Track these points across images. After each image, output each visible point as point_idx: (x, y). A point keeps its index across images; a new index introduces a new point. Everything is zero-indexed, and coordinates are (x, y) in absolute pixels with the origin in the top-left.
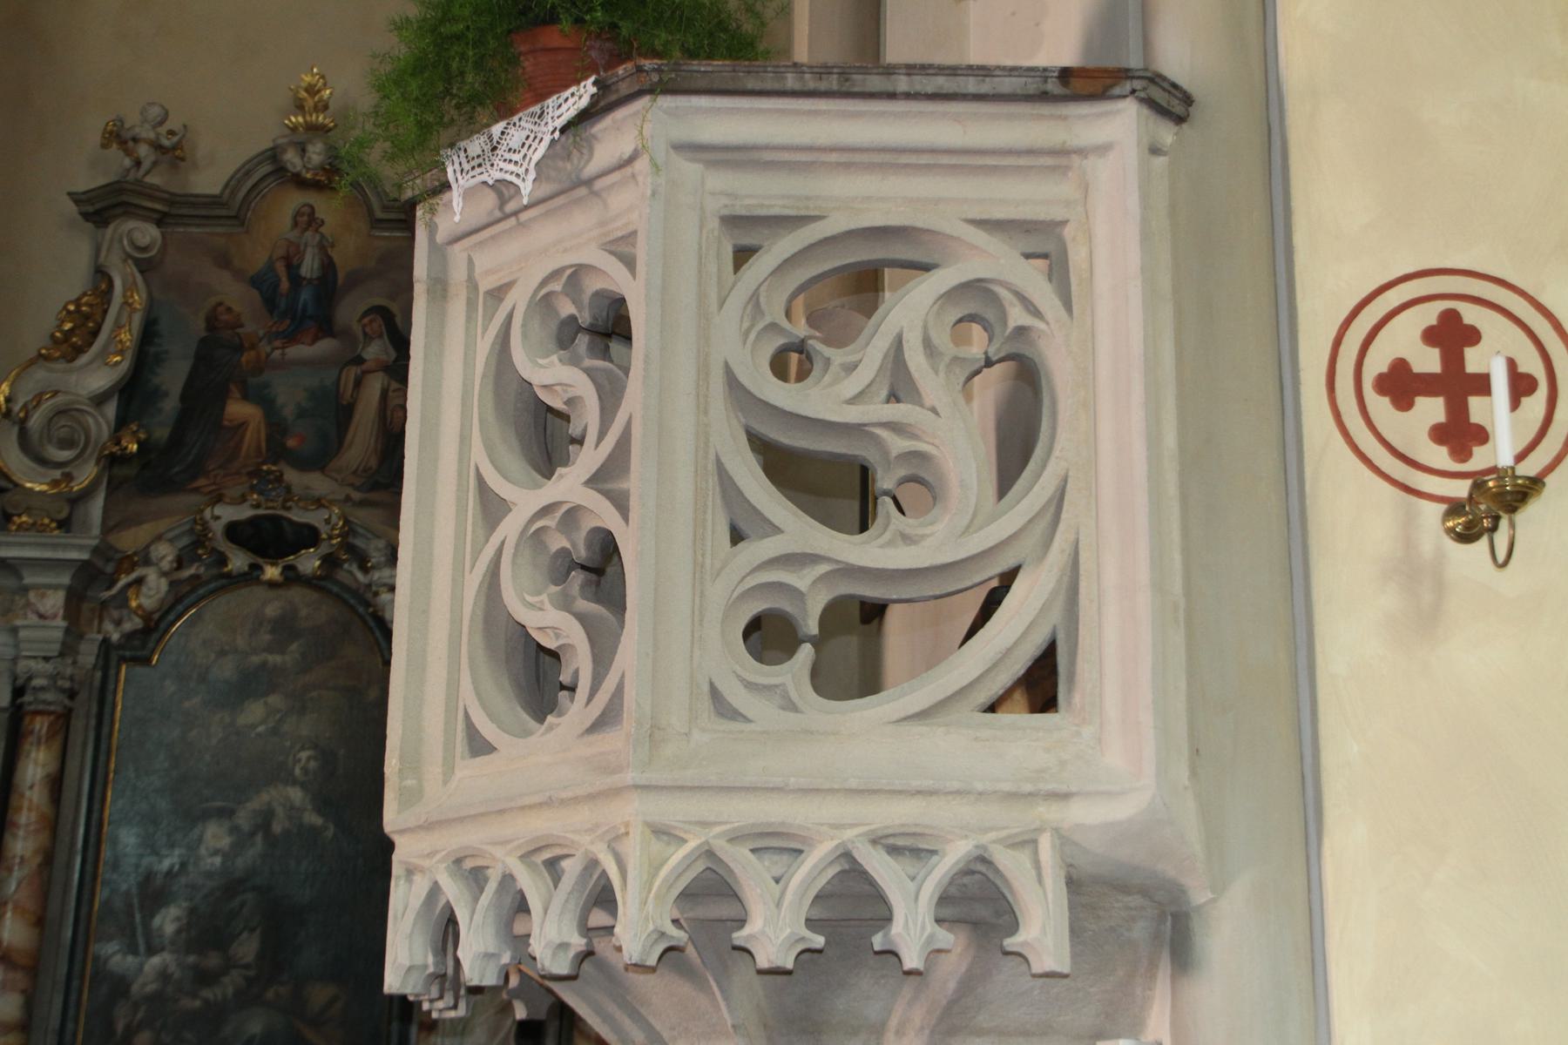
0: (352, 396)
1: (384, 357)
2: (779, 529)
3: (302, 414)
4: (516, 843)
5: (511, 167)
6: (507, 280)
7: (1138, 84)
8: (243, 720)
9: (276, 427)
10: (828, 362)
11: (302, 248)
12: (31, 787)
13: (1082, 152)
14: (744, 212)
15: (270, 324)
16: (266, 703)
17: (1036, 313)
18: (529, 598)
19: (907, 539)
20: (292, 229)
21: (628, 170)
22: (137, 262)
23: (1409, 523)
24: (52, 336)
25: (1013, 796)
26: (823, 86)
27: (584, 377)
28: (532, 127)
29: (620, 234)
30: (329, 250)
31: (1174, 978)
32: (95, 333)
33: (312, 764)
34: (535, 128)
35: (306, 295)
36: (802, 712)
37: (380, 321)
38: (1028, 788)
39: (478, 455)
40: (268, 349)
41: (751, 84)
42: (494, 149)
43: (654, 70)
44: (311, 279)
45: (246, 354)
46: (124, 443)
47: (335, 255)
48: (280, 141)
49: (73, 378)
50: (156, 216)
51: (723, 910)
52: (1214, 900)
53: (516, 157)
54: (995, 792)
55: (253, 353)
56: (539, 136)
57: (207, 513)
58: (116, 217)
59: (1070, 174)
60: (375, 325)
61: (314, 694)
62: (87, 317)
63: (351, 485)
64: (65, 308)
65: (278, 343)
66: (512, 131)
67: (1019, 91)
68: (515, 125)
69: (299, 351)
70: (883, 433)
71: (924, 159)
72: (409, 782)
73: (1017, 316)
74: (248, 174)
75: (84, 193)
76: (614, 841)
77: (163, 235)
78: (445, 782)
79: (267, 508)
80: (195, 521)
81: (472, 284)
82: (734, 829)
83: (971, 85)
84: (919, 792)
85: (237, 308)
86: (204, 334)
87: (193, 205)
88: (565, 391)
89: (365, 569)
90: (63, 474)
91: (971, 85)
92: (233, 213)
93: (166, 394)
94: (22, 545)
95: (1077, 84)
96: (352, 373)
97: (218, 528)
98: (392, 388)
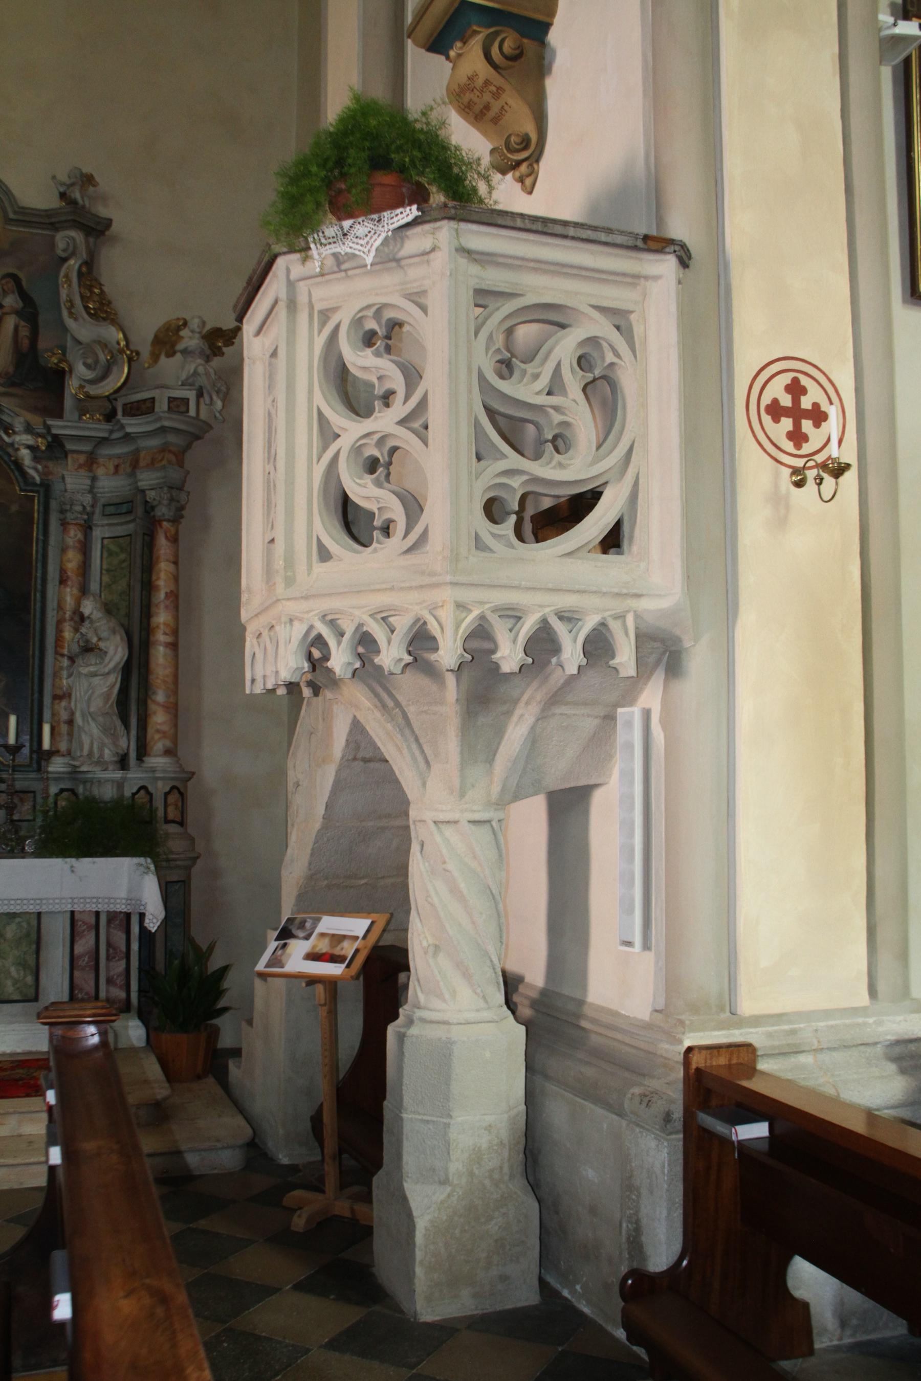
2: (505, 456)
4: (369, 608)
5: (359, 247)
6: (335, 305)
7: (677, 248)
10: (524, 372)
13: (646, 278)
14: (486, 288)
17: (617, 355)
18: (358, 481)
19: (561, 465)
21: (426, 257)
23: (777, 475)
25: (618, 595)
26: (534, 227)
27: (394, 366)
28: (373, 227)
29: (415, 290)
31: (666, 680)
34: (375, 228)
36: (516, 549)
38: (625, 591)
39: (319, 400)
41: (500, 222)
42: (345, 235)
43: (453, 207)
51: (486, 645)
52: (694, 646)
53: (361, 242)
54: (611, 593)
56: (378, 232)
59: (638, 288)
66: (357, 226)
67: (625, 244)
68: (359, 223)
70: (551, 411)
71: (575, 271)
72: (289, 574)
73: (610, 358)
76: (432, 610)
78: (309, 574)
81: (311, 306)
82: (496, 606)
83: (603, 237)
84: (578, 591)
88: (378, 372)
89: (9, 435)
91: (603, 237)
95: (651, 244)
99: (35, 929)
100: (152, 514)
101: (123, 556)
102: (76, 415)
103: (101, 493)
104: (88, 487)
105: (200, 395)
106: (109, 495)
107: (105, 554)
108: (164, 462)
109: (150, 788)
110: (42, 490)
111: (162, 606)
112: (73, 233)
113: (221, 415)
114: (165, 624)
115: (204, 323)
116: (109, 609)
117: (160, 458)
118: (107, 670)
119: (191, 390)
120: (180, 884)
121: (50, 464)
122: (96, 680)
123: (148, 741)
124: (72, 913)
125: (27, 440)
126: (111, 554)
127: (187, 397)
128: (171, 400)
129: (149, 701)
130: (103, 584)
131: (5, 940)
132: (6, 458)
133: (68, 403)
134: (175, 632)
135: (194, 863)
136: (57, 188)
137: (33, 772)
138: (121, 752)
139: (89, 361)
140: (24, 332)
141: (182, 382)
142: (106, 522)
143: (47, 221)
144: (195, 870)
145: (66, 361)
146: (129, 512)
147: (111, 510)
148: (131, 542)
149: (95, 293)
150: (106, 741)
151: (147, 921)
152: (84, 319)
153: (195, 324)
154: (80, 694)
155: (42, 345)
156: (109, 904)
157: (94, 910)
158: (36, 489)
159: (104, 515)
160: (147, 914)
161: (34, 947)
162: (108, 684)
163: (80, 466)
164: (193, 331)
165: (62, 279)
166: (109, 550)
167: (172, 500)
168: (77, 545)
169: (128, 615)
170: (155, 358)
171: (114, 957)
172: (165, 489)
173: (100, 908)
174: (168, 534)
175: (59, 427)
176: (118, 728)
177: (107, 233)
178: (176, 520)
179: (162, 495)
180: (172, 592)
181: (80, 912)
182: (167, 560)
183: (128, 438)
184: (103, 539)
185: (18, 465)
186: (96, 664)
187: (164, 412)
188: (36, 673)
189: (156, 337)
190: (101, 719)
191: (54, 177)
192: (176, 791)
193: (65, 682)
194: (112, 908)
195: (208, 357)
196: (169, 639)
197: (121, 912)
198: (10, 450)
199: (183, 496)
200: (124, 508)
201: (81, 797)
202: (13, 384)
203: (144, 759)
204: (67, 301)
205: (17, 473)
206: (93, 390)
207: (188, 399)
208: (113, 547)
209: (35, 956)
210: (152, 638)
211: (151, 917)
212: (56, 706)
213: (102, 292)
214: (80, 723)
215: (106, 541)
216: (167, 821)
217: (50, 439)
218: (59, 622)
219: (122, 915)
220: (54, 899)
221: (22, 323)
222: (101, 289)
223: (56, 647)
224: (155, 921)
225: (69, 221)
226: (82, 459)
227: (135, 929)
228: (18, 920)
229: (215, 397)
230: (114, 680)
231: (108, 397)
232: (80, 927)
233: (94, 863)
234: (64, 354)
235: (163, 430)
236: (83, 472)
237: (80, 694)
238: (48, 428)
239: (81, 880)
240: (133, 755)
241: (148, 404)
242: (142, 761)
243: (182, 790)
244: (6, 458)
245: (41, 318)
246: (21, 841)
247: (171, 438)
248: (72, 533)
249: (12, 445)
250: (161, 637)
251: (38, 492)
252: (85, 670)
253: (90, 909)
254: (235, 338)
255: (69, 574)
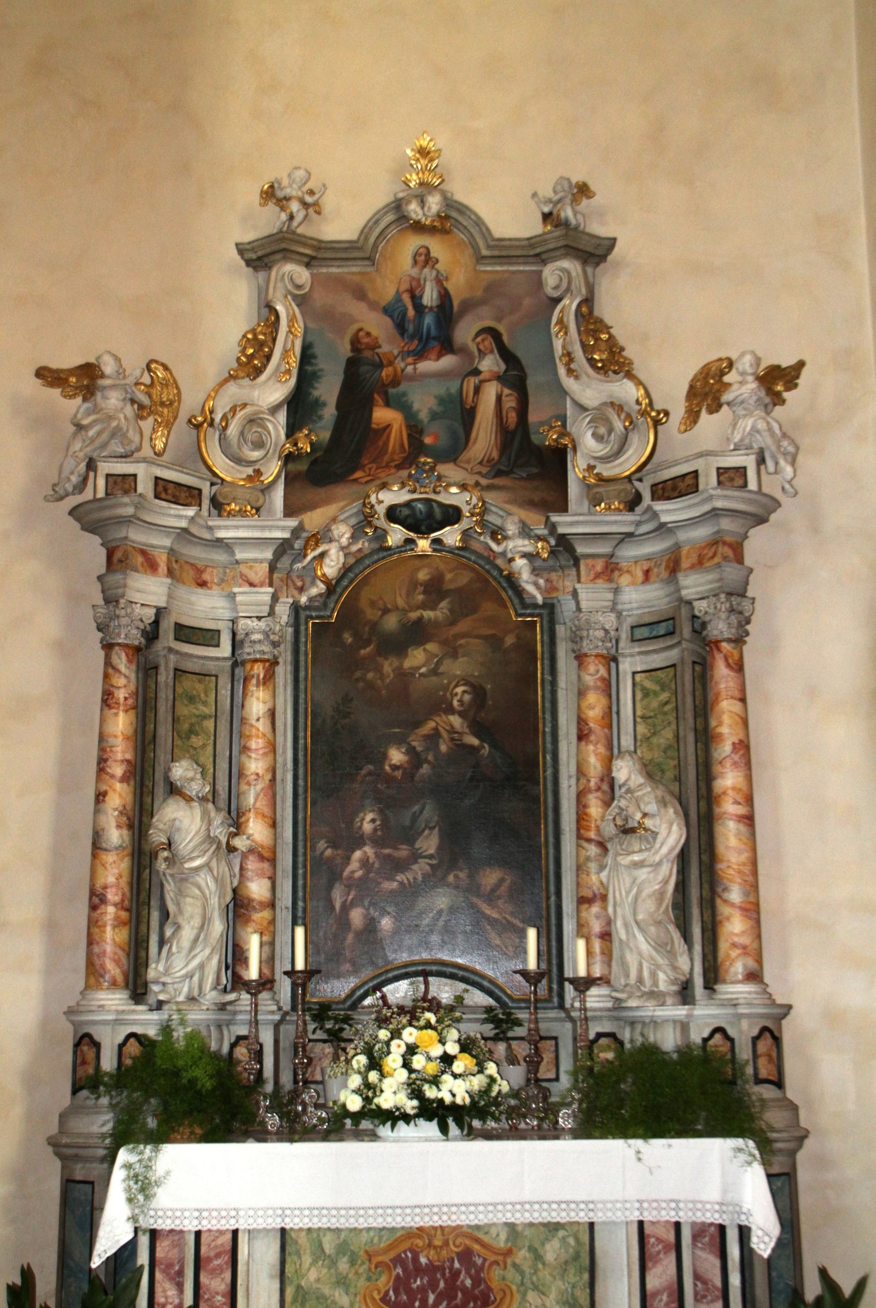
0: (473, 401)
1: (496, 369)
3: (434, 416)
8: (408, 664)
9: (415, 430)
11: (422, 282)
12: (258, 720)
15: (403, 344)
16: (425, 650)
20: (413, 267)
22: (295, 297)
24: (238, 359)
30: (445, 283)
32: (268, 357)
33: (467, 698)
35: (429, 320)
37: (490, 339)
40: (402, 365)
44: (431, 308)
45: (385, 369)
46: (300, 445)
47: (450, 286)
48: (401, 195)
49: (256, 393)
50: (306, 260)
55: (390, 369)
57: (373, 499)
58: (278, 261)
60: (487, 343)
61: (462, 641)
62: (262, 344)
63: (480, 473)
64: (244, 336)
65: (410, 360)
69: (427, 366)
74: (377, 222)
75: (249, 243)
77: (313, 276)
79: (421, 493)
80: (364, 505)
85: (374, 333)
86: (350, 354)
87: (334, 249)
89: (498, 542)
90: (254, 471)
92: (367, 255)
93: (324, 404)
94: (237, 527)
96: (473, 381)
97: (381, 510)
98: (505, 394)
99: (587, 1248)
100: (705, 633)
101: (664, 696)
102: (586, 503)
103: (628, 610)
104: (610, 603)
105: (761, 461)
106: (640, 612)
107: (639, 695)
108: (717, 560)
109: (731, 1032)
110: (544, 612)
111: (728, 763)
112: (566, 264)
113: (792, 486)
114: (734, 789)
115: (758, 360)
116: (651, 771)
117: (711, 554)
118: (657, 858)
119: (747, 455)
120: (783, 1178)
121: (554, 576)
122: (643, 874)
123: (720, 960)
124: (641, 1224)
125: (524, 546)
126: (646, 693)
127: (743, 465)
128: (721, 472)
129: (719, 902)
130: (639, 737)
131: (544, 1264)
132: (495, 573)
133: (574, 489)
134: (749, 800)
135: (800, 1146)
136: (539, 207)
137: (553, 1008)
138: (683, 979)
139: (602, 430)
140: (510, 403)
141: (735, 444)
142: (637, 650)
143: (532, 253)
144: (801, 1156)
145: (568, 434)
146: (671, 633)
147: (644, 632)
148: (675, 675)
149: (601, 339)
150: (660, 961)
151: (754, 1239)
152: (588, 376)
153: (745, 363)
154: (621, 894)
155: (533, 417)
156: (694, 1210)
157: (674, 1220)
158: (537, 611)
159: (633, 641)
160: (754, 1228)
161: (586, 1276)
162: (660, 878)
163: (597, 576)
164: (743, 374)
165: (554, 329)
166: (643, 689)
167: (732, 610)
168: (599, 684)
169: (678, 779)
170: (692, 417)
171: (704, 1297)
172: (723, 596)
173: (684, 1217)
174: (730, 661)
175: (566, 524)
176: (676, 942)
177: (609, 258)
178: (739, 641)
179: (719, 606)
180: (741, 741)
181: (653, 1223)
182: (732, 698)
183: (662, 529)
184: (634, 673)
185: (512, 581)
186: (641, 851)
187: (713, 489)
188: (552, 867)
189: (692, 387)
190: (653, 929)
191: (535, 195)
192: (768, 1035)
193: (594, 878)
194: (700, 1217)
195: (766, 406)
196: (741, 810)
197: (712, 1224)
198: (499, 562)
199: (746, 605)
200: (662, 629)
201: (628, 1046)
202: (499, 474)
203: (716, 987)
204: (563, 355)
205: (510, 593)
206: (606, 470)
207: (745, 468)
208: (648, 684)
209: (588, 1290)
210: (717, 810)
211: (760, 1233)
212: (584, 914)
213: (611, 337)
214: (623, 936)
215: (638, 677)
216: (759, 1081)
217: (553, 542)
218: (581, 795)
219: (712, 1229)
220: (614, 1202)
221: (506, 391)
222: (608, 333)
223: (578, 829)
224: (766, 1239)
225: (560, 247)
226: (599, 565)
227: (734, 1251)
228: (561, 1233)
229: (782, 462)
230: (668, 873)
231: (629, 478)
232: (653, 1246)
233: (670, 1146)
234: (564, 425)
235: (715, 513)
236: (601, 584)
237: (621, 894)
238: (552, 528)
239: (651, 1173)
240: (698, 981)
241: (689, 481)
242: (714, 990)
243: (776, 1033)
244: (495, 573)
245: (531, 382)
246: (550, 1111)
247: (726, 524)
248: (592, 669)
249: (503, 554)
250: (730, 807)
251: (539, 615)
252: (625, 860)
253: (668, 1218)
254: (798, 377)
255: (592, 725)
